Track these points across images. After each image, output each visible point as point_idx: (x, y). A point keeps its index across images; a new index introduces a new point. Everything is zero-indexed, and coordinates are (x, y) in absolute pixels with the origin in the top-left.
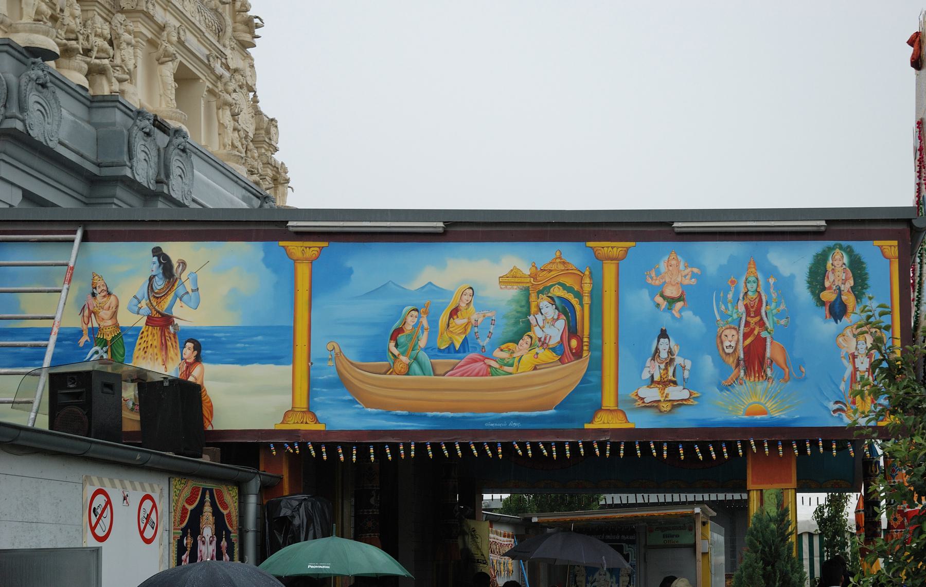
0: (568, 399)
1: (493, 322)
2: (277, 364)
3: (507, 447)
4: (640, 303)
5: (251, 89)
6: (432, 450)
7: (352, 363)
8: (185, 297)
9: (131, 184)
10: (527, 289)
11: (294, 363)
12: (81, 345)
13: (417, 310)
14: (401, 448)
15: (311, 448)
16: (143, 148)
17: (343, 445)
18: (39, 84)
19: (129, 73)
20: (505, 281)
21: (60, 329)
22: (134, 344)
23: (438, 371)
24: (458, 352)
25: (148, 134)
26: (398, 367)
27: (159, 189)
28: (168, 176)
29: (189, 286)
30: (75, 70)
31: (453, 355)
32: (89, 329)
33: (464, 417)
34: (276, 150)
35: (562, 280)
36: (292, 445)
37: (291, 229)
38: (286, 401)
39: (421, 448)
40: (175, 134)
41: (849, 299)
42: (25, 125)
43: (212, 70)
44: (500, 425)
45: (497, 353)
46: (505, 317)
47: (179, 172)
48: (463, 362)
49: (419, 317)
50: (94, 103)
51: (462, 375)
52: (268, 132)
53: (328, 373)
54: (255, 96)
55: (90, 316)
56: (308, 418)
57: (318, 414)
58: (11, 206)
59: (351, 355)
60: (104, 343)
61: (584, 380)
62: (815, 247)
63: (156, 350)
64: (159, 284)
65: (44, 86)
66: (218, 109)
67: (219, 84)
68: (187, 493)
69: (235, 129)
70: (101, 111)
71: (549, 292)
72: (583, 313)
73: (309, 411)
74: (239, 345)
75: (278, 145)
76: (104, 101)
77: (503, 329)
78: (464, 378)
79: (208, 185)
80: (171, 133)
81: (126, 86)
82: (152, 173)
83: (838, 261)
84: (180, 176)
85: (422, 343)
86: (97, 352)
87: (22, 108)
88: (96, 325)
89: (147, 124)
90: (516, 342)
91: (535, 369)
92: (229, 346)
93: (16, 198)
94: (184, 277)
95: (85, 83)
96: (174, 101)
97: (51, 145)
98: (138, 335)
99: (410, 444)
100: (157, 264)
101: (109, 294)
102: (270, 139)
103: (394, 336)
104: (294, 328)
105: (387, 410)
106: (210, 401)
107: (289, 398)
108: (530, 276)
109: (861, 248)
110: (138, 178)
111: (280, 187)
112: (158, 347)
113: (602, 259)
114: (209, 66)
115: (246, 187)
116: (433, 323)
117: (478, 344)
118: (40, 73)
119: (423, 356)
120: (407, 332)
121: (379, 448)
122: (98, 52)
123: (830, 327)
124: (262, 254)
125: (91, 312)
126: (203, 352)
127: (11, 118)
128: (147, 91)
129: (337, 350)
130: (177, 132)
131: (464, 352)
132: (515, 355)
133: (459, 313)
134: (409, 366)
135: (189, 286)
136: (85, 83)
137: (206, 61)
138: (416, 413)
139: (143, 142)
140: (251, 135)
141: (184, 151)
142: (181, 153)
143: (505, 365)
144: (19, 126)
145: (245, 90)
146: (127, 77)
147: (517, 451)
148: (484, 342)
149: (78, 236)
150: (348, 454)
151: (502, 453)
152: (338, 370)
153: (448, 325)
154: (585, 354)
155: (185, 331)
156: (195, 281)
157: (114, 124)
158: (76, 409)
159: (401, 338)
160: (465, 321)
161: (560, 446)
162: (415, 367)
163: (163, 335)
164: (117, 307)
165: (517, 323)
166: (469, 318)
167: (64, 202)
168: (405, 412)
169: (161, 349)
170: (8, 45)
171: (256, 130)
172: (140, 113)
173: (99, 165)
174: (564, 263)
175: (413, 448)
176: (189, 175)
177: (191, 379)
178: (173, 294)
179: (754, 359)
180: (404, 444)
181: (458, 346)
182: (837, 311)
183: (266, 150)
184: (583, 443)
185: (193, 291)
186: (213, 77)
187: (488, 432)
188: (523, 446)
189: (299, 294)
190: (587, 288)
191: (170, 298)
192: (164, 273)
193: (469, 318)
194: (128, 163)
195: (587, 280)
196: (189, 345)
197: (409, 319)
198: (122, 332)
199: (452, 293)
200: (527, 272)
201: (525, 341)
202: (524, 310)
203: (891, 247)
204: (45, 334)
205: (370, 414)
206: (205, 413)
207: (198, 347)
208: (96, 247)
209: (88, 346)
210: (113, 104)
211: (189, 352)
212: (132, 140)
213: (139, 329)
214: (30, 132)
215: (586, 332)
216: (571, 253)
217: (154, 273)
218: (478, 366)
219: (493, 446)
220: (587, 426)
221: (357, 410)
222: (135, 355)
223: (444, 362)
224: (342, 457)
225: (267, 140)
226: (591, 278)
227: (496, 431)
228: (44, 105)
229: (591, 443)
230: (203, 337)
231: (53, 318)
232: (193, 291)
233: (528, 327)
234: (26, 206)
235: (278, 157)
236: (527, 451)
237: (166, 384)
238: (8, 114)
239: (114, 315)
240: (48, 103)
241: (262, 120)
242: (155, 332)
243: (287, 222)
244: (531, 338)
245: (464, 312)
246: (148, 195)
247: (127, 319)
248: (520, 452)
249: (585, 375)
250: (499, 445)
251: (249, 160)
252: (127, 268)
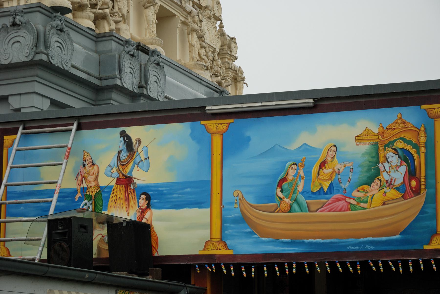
0: (410, 227)
1: (351, 170)
2: (200, 207)
3: (364, 264)
5: (218, 19)
6: (308, 268)
7: (251, 205)
8: (141, 164)
9: (122, 90)
10: (377, 144)
11: (211, 207)
12: (76, 200)
13: (295, 164)
14: (286, 266)
15: (223, 267)
16: (129, 65)
17: (245, 265)
18: (58, 30)
19: (123, 16)
20: (359, 139)
21: (60, 190)
22: (108, 198)
23: (312, 209)
24: (326, 194)
25: (133, 56)
26: (284, 206)
27: (141, 92)
28: (146, 83)
29: (143, 156)
30: (86, 18)
31: (322, 196)
32: (81, 189)
33: (332, 243)
34: (236, 58)
35: (403, 135)
36: (210, 266)
37: (208, 112)
38: (205, 234)
39: (300, 266)
40: (152, 54)
42: (48, 57)
43: (184, 9)
44: (358, 248)
45: (355, 194)
46: (361, 166)
47: (155, 79)
48: (330, 201)
49: (297, 169)
50: (98, 38)
51: (329, 211)
52: (229, 47)
53: (236, 214)
54: (221, 23)
55: (82, 180)
56: (221, 246)
57: (228, 242)
58: (42, 110)
59: (250, 199)
60: (90, 198)
61: (422, 212)
63: (122, 201)
64: (124, 155)
65: (61, 30)
66: (189, 34)
67: (189, 18)
69: (202, 47)
70: (103, 43)
71: (393, 145)
72: (420, 160)
73: (222, 241)
74: (175, 195)
75: (237, 55)
76: (105, 37)
77: (359, 175)
78: (331, 213)
79: (178, 87)
80: (150, 53)
81: (122, 26)
82: (136, 82)
84: (156, 82)
85: (300, 189)
86: (86, 204)
87: (47, 46)
88: (85, 186)
89: (132, 49)
90: (369, 184)
91: (384, 204)
92: (169, 196)
93: (45, 105)
94: (140, 150)
95: (92, 26)
96: (155, 32)
97: (66, 68)
98: (110, 192)
99: (292, 263)
100: (123, 142)
101: (94, 164)
102: (231, 52)
103: (280, 184)
104: (211, 182)
105: (276, 239)
106: (156, 236)
107: (209, 231)
108: (378, 134)
110: (125, 86)
111: (238, 84)
112: (124, 199)
113: (433, 118)
114: (181, 7)
115: (208, 85)
116: (308, 173)
117: (341, 188)
118: (59, 22)
119: (301, 198)
120: (289, 181)
121: (271, 267)
122: (102, 5)
124: (189, 131)
125: (83, 177)
126: (152, 201)
127: (39, 53)
128: (136, 28)
129: (241, 196)
130: (154, 52)
131: (331, 193)
132: (368, 194)
133: (326, 165)
134: (291, 206)
135: (143, 156)
136: (92, 26)
137: (179, 4)
138: (297, 241)
139: (129, 61)
140: (218, 50)
141: (158, 64)
142: (156, 66)
143: (361, 202)
144: (44, 58)
145: (213, 20)
146: (121, 19)
147: (372, 267)
148: (345, 185)
149: (74, 127)
150: (249, 272)
151: (360, 269)
152: (242, 211)
153: (319, 174)
154: (422, 191)
155: (141, 187)
156: (147, 152)
157: (111, 51)
158: (63, 244)
159: (285, 185)
160: (331, 170)
161: (405, 263)
162: (295, 206)
163: (126, 191)
164: (98, 173)
165: (369, 170)
166: (334, 168)
167: (77, 104)
168: (288, 240)
169: (126, 201)
170: (40, 7)
171: (221, 46)
172: (127, 42)
173: (100, 79)
174: (404, 123)
175: (294, 266)
176: (163, 81)
177: (144, 221)
178: (132, 162)
180: (288, 264)
181: (326, 189)
183: (229, 59)
184: (423, 261)
185: (145, 159)
186: (185, 13)
187: (349, 254)
188: (376, 263)
189: (215, 157)
190: (423, 140)
191: (131, 165)
192: (127, 148)
193: (334, 168)
194: (118, 76)
195: (422, 134)
196: (143, 197)
197: (291, 171)
198: (101, 190)
199: (321, 150)
200: (376, 131)
201: (376, 184)
202: (375, 160)
204: (51, 193)
205: (263, 242)
206: (154, 244)
207: (148, 198)
208: (85, 133)
209: (80, 200)
210: (110, 38)
211: (143, 202)
212: (121, 60)
213: (111, 187)
214: (52, 61)
215: (423, 175)
216: (410, 115)
217: (121, 149)
218: (341, 203)
219: (354, 264)
220: (426, 247)
221: (255, 240)
222: (109, 206)
223: (315, 202)
224: (244, 274)
225: (229, 52)
226: (425, 132)
227: (356, 253)
228: (62, 43)
229: (429, 261)
230: (152, 191)
231: (56, 183)
232: (145, 159)
233: (378, 172)
234: (53, 109)
235: (237, 63)
236: (379, 267)
237: (125, 224)
238: (38, 51)
239: (97, 178)
240: (65, 41)
241: (225, 39)
242: (121, 189)
243: (205, 107)
244: (380, 181)
245: (330, 164)
246: (133, 96)
247: (106, 181)
248: (374, 268)
249: (423, 207)
250: (358, 263)
251: (215, 67)
252: (104, 145)
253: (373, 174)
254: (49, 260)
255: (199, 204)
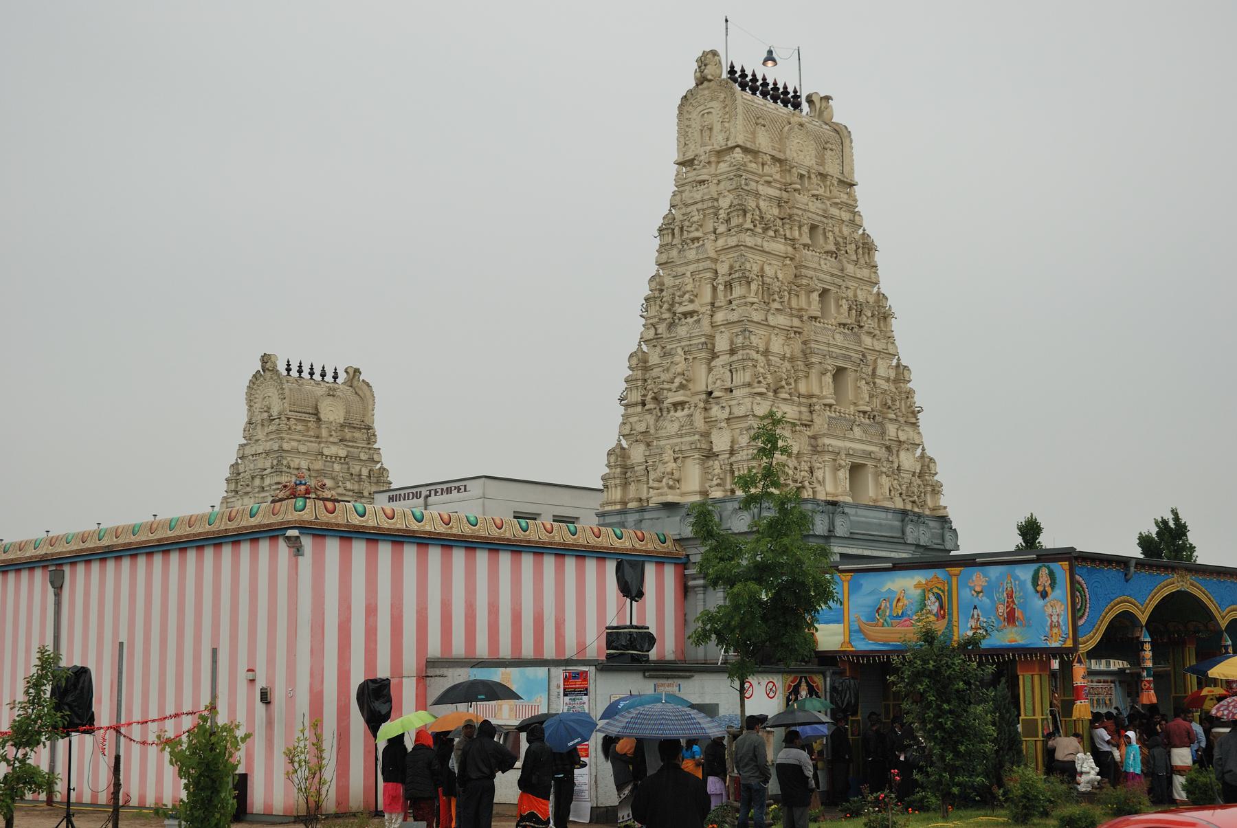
4: (966, 594)
20: (916, 587)
38: (840, 639)
41: (1048, 589)
53: (856, 628)
59: (863, 619)
62: (1035, 566)
68: (791, 678)
72: (945, 599)
77: (914, 608)
82: (826, 528)
83: (1044, 572)
105: (876, 642)
109: (1053, 565)
121: (874, 657)
123: (1041, 602)
179: (1011, 618)
182: (1044, 595)
203: (1066, 564)
216: (939, 573)
253: (923, 605)
254: (403, 782)
255: (838, 622)
